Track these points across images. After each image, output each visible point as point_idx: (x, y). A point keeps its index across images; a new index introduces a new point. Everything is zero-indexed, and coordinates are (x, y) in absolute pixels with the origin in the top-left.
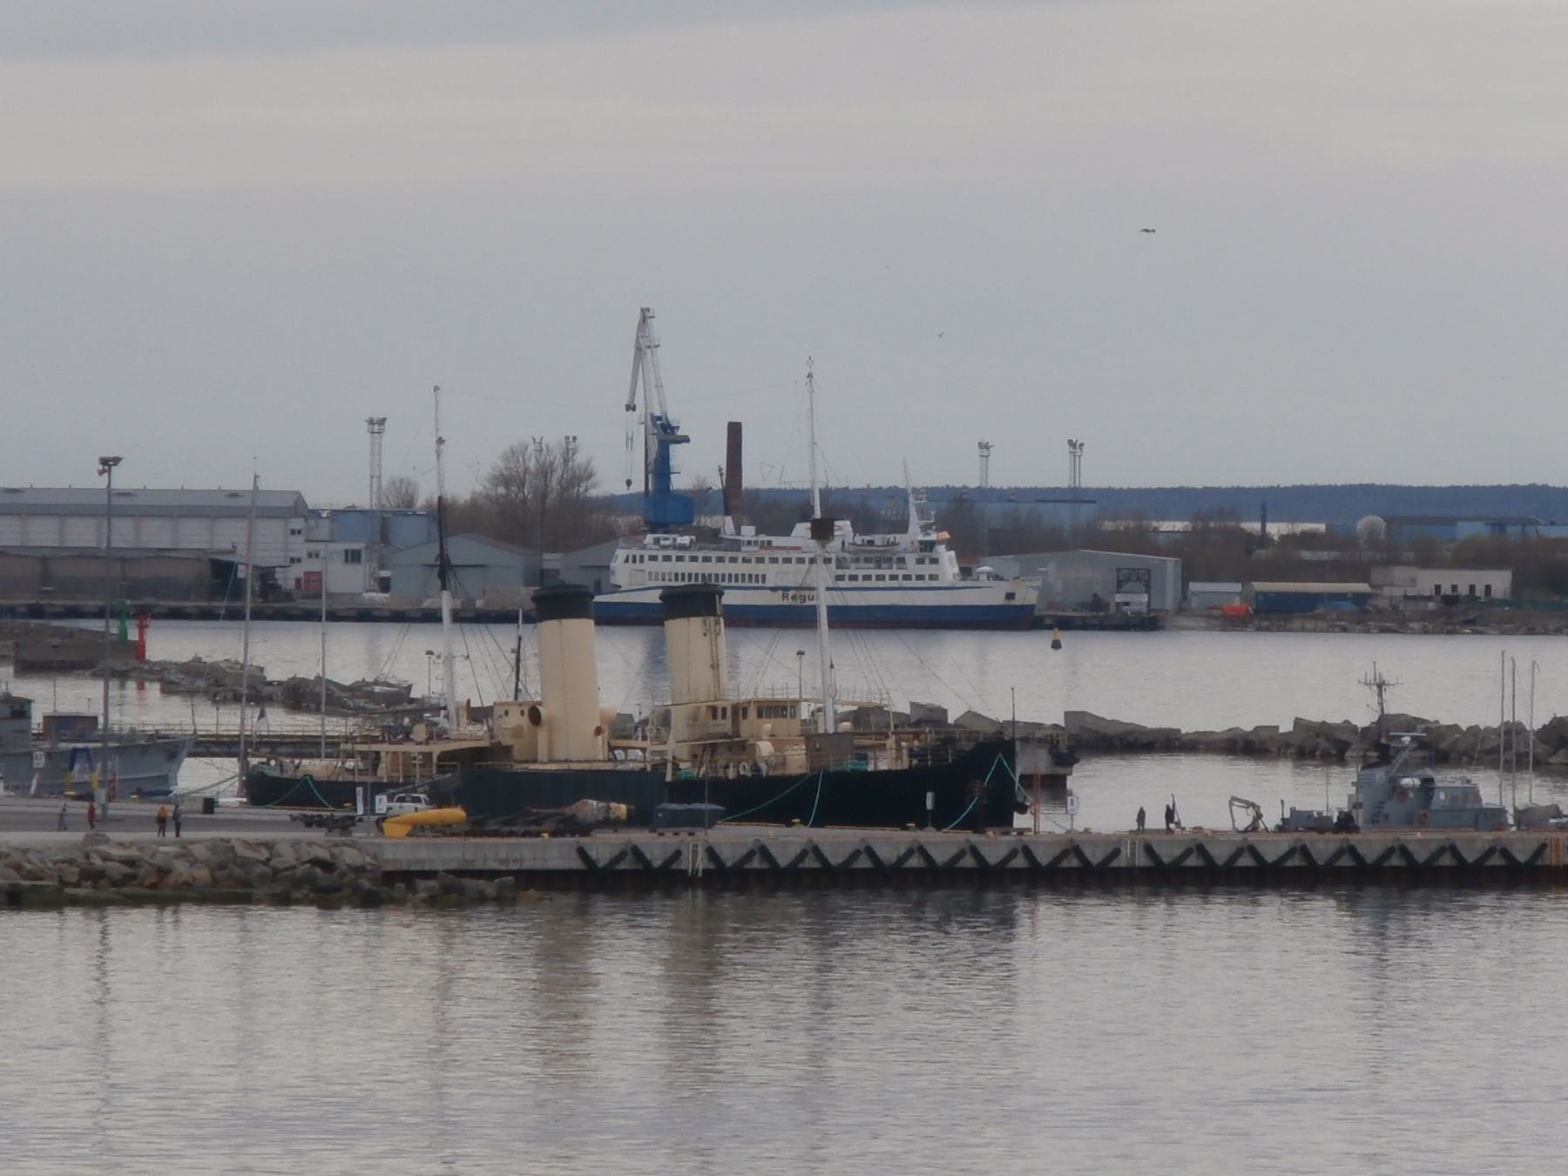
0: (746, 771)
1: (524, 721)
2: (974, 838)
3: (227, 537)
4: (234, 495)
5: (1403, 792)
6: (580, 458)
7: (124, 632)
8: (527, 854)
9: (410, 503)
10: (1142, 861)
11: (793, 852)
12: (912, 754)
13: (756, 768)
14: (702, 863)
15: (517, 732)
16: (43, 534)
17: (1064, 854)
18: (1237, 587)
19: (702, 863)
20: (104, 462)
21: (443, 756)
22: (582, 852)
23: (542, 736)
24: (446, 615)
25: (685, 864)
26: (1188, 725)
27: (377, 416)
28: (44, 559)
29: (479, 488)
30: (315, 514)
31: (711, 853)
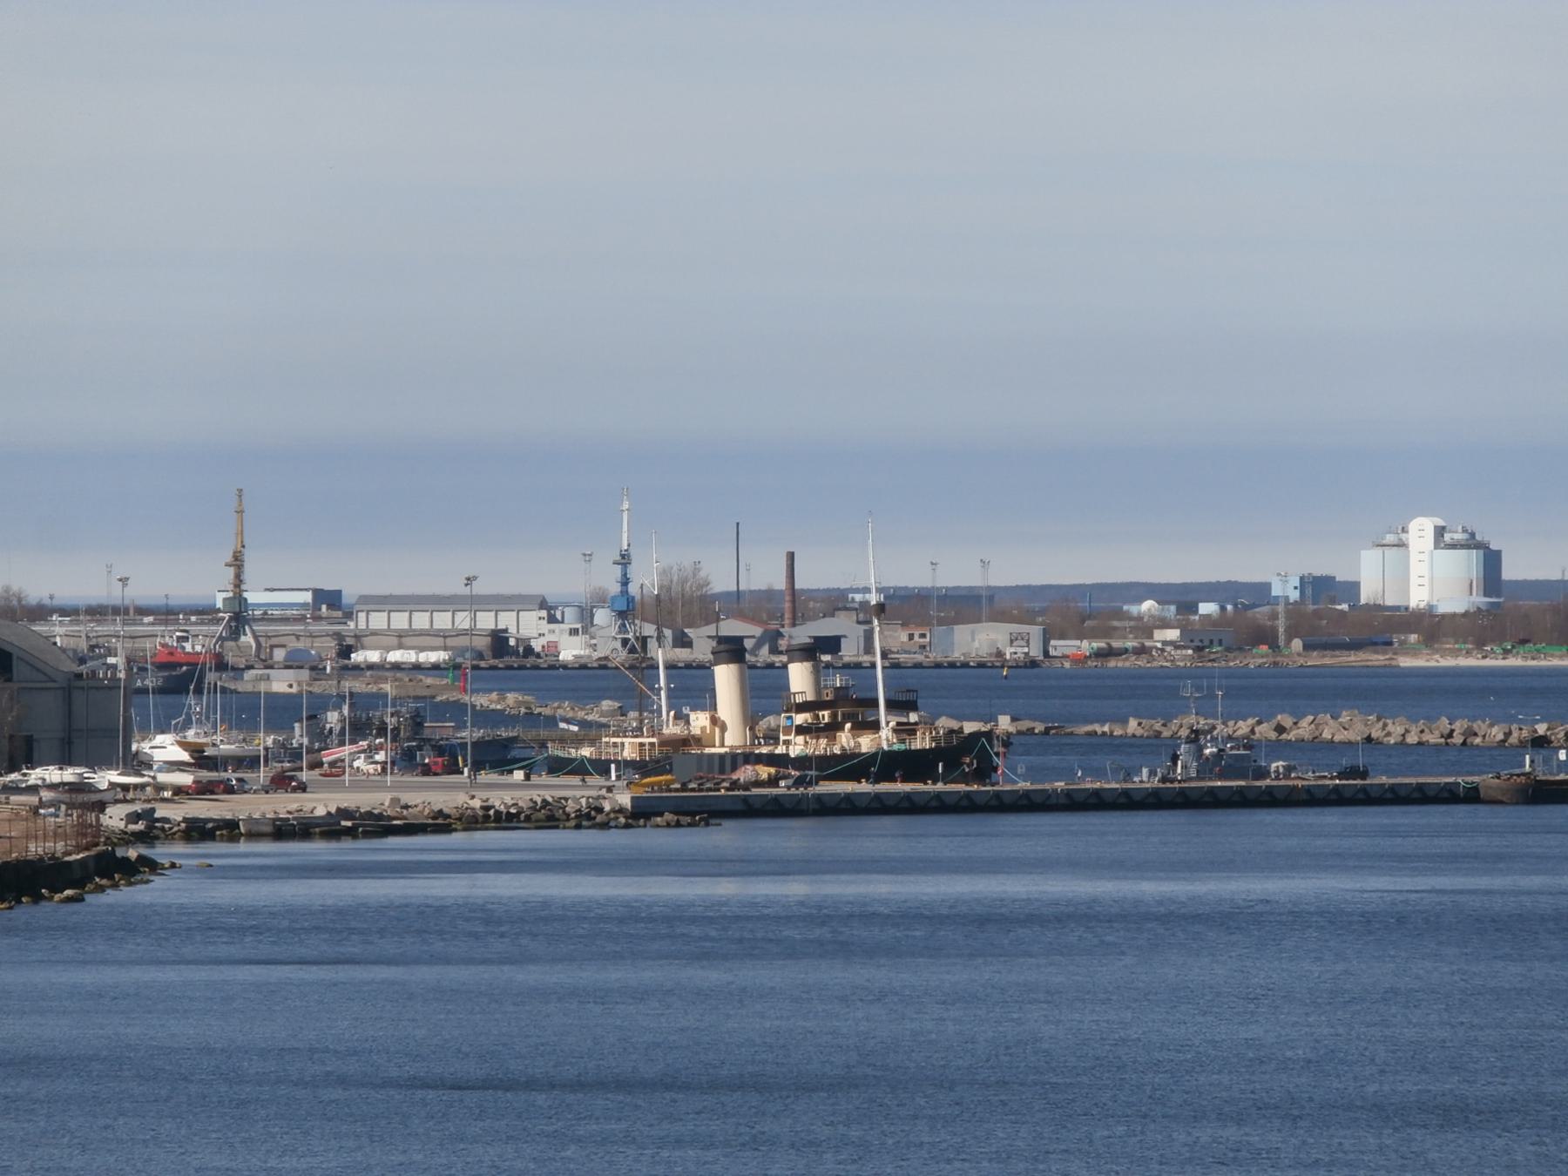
6: (702, 574)
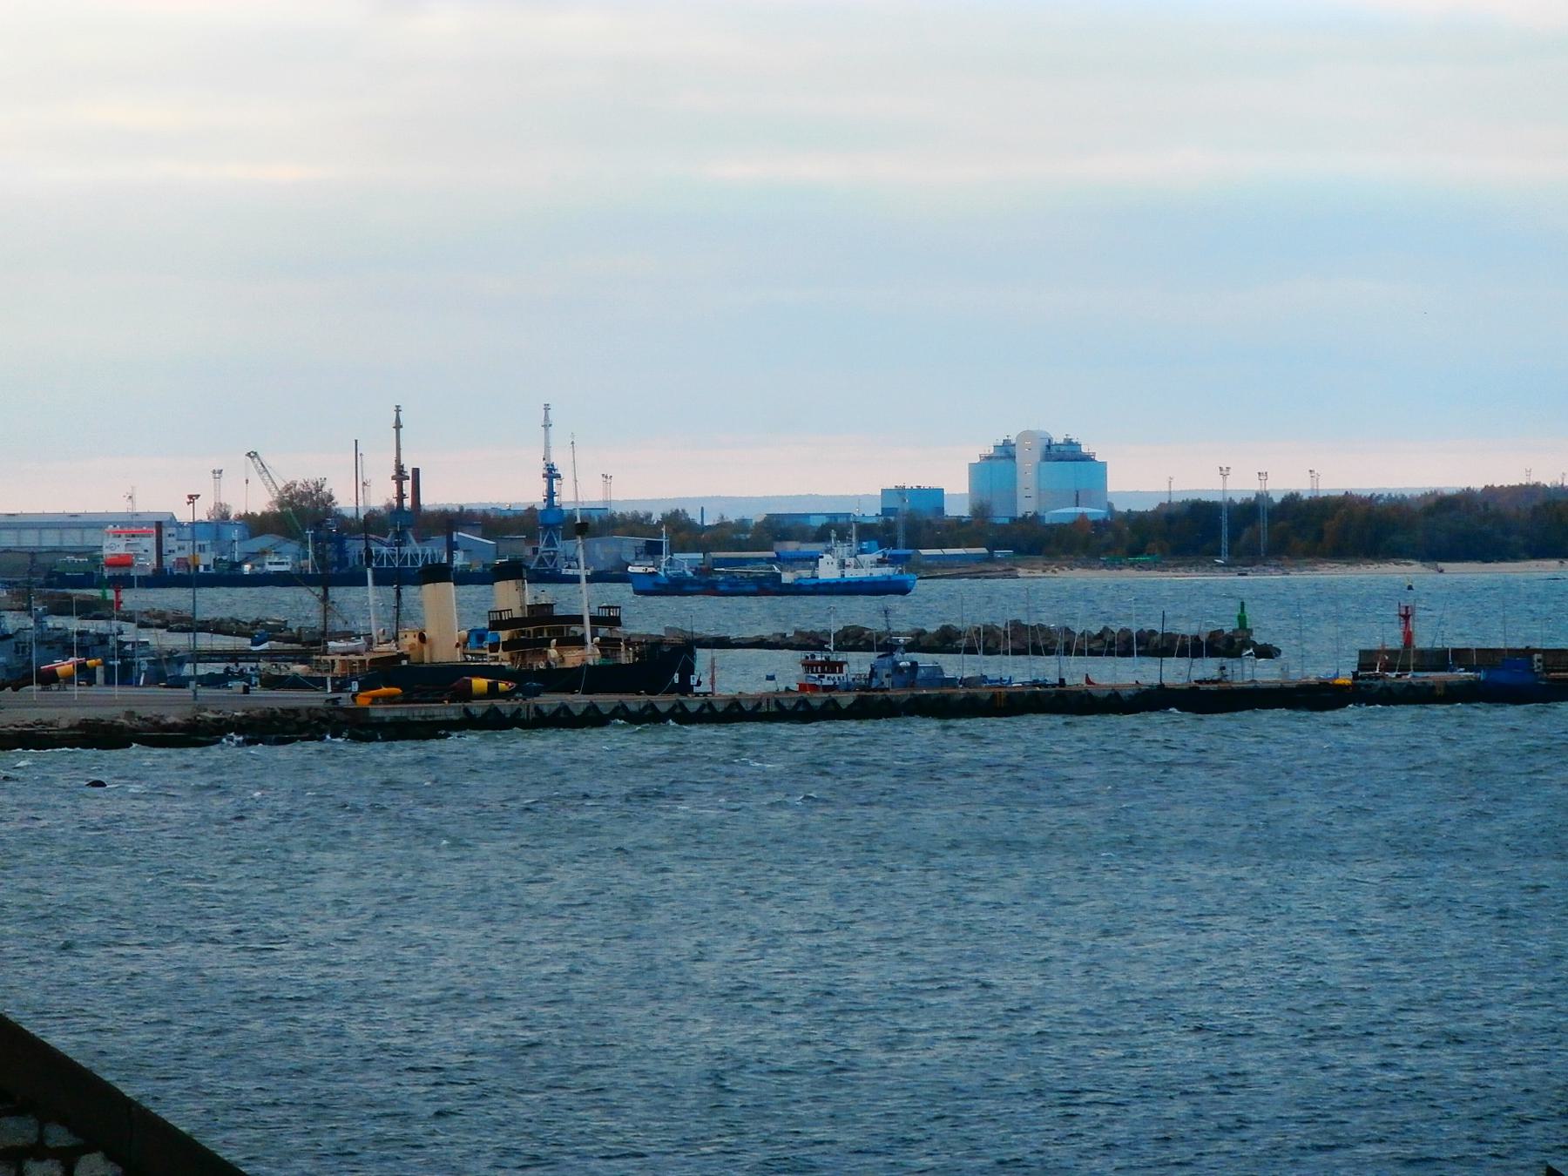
0: (542, 666)
1: (416, 640)
2: (682, 698)
3: (91, 539)
4: (75, 516)
5: (901, 670)
7: (104, 595)
8: (436, 712)
9: (225, 516)
10: (773, 709)
11: (582, 708)
12: (635, 654)
13: (548, 664)
14: (533, 715)
15: (412, 647)
16: (30, 540)
17: (731, 706)
18: (701, 555)
19: (533, 715)
20: (190, 497)
21: (372, 661)
22: (466, 710)
23: (426, 648)
24: (583, 579)
25: (524, 715)
26: (733, 635)
27: (217, 468)
28: (33, 554)
29: (266, 509)
30: (180, 525)
31: (537, 708)
